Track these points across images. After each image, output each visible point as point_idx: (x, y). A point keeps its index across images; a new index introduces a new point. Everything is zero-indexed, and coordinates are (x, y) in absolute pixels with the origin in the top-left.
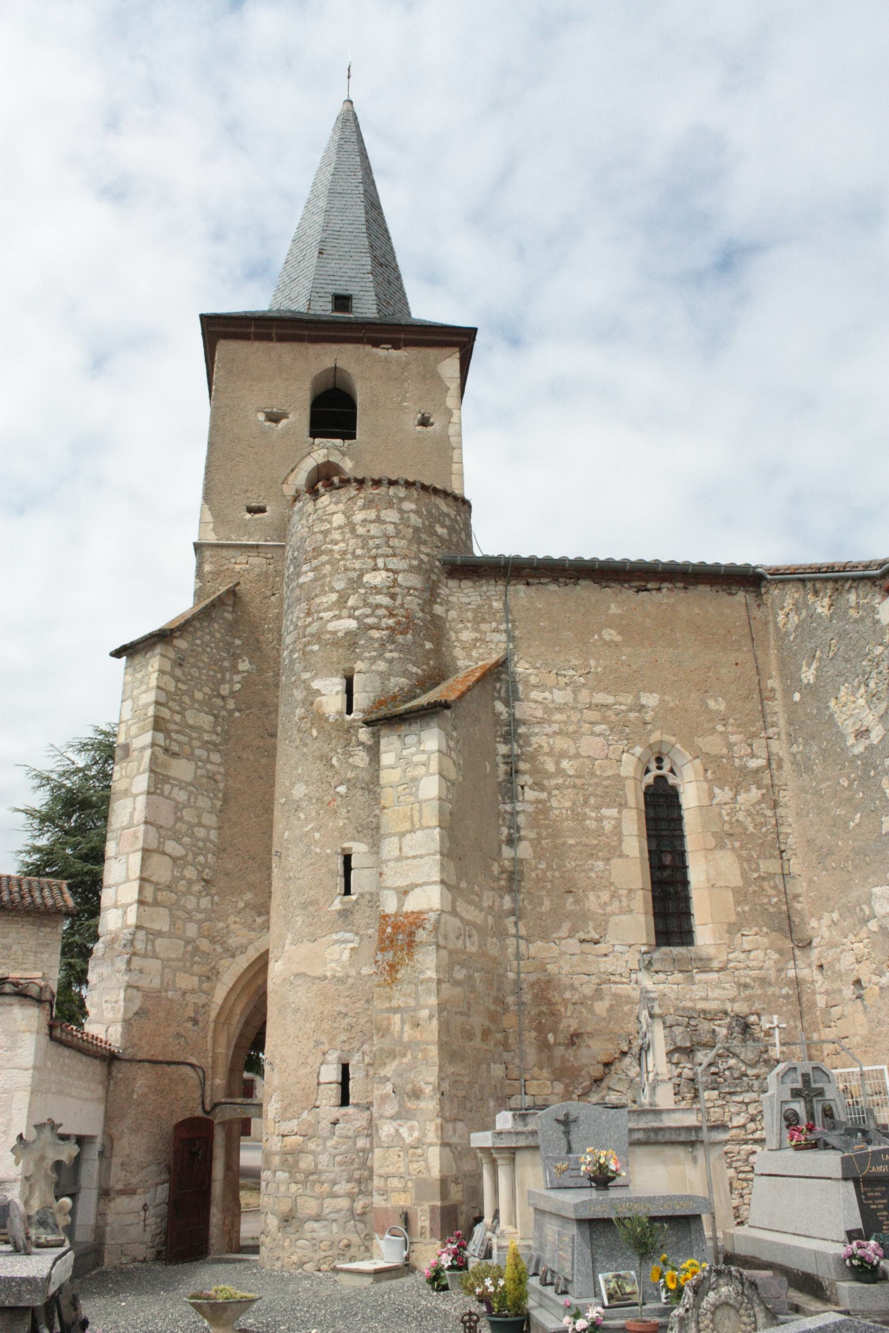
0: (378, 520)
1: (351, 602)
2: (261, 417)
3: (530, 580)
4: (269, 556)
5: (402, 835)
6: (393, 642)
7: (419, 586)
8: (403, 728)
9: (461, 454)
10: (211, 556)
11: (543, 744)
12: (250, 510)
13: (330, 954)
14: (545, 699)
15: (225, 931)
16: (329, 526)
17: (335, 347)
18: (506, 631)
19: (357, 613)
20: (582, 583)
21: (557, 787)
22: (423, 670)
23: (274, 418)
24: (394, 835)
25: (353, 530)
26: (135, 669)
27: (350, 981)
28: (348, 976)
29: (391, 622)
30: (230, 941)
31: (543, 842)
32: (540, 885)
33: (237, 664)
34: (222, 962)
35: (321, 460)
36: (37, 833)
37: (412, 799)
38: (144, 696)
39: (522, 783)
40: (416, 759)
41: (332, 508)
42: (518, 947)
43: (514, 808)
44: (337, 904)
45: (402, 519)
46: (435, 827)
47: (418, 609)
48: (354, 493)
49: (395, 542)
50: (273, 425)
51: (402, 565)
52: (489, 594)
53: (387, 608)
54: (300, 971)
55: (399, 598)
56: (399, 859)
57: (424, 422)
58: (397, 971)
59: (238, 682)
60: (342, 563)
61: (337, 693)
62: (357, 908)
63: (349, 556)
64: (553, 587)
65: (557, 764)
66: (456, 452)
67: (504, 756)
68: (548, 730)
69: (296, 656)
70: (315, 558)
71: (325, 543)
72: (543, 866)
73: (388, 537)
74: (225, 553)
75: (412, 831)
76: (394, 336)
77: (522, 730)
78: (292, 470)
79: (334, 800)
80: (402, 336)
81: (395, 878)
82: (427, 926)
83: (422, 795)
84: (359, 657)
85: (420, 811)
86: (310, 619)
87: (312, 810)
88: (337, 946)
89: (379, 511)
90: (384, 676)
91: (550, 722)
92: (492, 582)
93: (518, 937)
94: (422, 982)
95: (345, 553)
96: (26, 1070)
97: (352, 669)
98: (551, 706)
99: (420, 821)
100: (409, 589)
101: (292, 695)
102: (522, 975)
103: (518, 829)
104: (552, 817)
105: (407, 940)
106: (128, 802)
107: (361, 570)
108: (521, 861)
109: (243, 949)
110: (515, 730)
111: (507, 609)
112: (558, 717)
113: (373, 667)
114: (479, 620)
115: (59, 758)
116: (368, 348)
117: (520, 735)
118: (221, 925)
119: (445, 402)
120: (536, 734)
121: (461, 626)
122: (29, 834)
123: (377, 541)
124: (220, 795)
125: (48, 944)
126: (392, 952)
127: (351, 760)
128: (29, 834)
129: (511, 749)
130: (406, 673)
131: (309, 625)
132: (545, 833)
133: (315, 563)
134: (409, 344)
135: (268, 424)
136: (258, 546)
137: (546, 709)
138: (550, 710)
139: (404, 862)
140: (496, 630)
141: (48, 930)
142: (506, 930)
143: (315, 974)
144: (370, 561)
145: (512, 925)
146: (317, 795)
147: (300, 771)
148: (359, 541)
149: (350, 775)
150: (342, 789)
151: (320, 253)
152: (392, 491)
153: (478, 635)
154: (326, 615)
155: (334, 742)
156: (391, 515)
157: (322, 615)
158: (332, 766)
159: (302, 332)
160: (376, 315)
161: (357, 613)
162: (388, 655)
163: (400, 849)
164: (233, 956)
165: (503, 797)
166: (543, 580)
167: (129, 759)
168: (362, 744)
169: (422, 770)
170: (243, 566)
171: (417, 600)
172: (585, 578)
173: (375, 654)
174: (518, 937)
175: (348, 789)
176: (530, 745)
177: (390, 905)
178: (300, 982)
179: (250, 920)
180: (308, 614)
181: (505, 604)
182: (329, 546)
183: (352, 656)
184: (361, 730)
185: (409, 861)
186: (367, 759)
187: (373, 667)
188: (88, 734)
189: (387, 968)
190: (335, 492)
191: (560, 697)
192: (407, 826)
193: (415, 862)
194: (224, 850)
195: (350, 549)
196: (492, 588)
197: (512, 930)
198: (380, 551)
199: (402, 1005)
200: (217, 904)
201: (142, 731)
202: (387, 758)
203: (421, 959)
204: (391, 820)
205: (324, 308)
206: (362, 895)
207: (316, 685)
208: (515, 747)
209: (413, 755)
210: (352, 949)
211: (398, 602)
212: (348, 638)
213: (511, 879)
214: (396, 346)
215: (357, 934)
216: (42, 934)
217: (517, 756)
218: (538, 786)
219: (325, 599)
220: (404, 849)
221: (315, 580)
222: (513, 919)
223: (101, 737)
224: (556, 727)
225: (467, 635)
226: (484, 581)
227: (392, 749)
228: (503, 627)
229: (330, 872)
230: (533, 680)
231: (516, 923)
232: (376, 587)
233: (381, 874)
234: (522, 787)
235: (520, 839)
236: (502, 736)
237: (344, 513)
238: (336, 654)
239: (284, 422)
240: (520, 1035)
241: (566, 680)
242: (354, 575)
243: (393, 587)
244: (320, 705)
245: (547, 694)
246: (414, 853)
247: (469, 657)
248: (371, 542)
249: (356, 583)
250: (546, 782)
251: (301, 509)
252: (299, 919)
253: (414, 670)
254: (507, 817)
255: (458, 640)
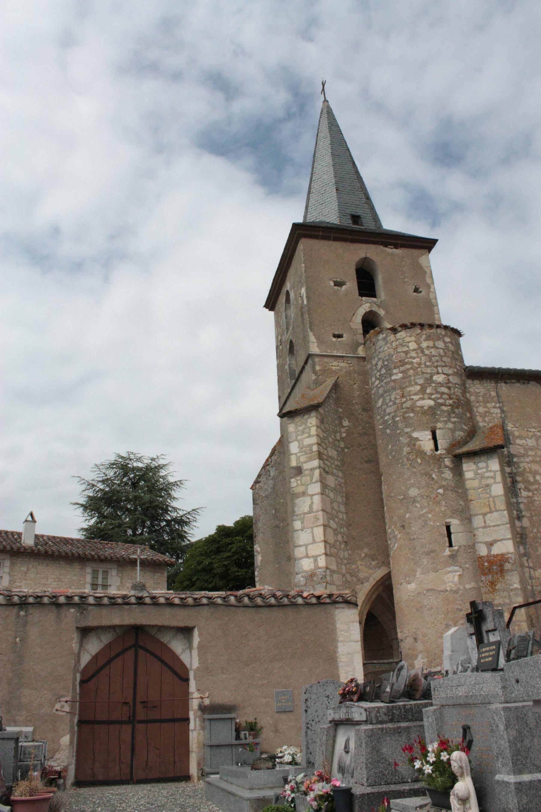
0: (435, 347)
1: (428, 391)
2: (332, 284)
3: (507, 381)
4: (349, 362)
5: (484, 515)
6: (454, 413)
7: (459, 383)
8: (476, 458)
9: (438, 309)
10: (319, 362)
11: (526, 467)
12: (335, 336)
13: (447, 578)
14: (523, 443)
15: (357, 570)
16: (407, 349)
17: (364, 246)
18: (499, 407)
19: (433, 397)
20: (532, 383)
21: (536, 490)
22: (469, 428)
23: (339, 284)
24: (480, 514)
25: (423, 352)
26: (296, 424)
27: (461, 592)
28: (459, 590)
29: (451, 402)
30: (360, 575)
31: (534, 518)
32: (536, 541)
33: (342, 422)
34: (357, 587)
35: (368, 310)
36: (89, 518)
37: (488, 496)
38: (307, 440)
39: (519, 488)
40: (486, 475)
41: (408, 339)
42: (530, 573)
43: (517, 501)
44: (447, 552)
45: (445, 346)
46: (504, 510)
47: (461, 395)
48: (420, 331)
49: (445, 359)
50: (339, 288)
51: (450, 371)
52: (488, 387)
53: (448, 394)
54: (430, 588)
55: (452, 389)
56: (485, 527)
57: (416, 290)
58: (496, 585)
59: (345, 432)
60: (419, 369)
61: (429, 440)
62: (459, 553)
63: (423, 366)
64: (518, 385)
65: (534, 477)
66: (435, 308)
67: (509, 473)
68: (528, 460)
69: (397, 419)
70: (402, 366)
71: (407, 358)
72: (535, 531)
73: (441, 357)
74: (326, 360)
75: (491, 512)
76: (394, 241)
77: (515, 460)
78: (354, 315)
79: (437, 497)
80: (400, 242)
81: (483, 536)
82: (510, 561)
83: (494, 493)
84: (438, 421)
85: (494, 502)
86: (404, 399)
87: (425, 502)
88: (450, 574)
89: (434, 341)
90: (453, 431)
91: (528, 456)
92: (489, 381)
93: (529, 567)
94: (512, 590)
95: (420, 364)
96: (357, 642)
97: (436, 427)
98: (527, 447)
99: (494, 507)
100: (456, 384)
101: (399, 440)
102: (534, 587)
103: (521, 512)
104: (536, 505)
105: (499, 568)
106: (307, 499)
107: (431, 373)
108: (525, 528)
109: (367, 579)
110: (512, 460)
111: (498, 396)
112: (530, 453)
113: (446, 426)
114: (486, 402)
115: (98, 472)
116: (382, 247)
117: (515, 462)
118: (354, 566)
119: (425, 280)
120: (522, 462)
121: (478, 404)
122: (84, 518)
123: (437, 358)
124: (344, 495)
125: (159, 583)
126: (491, 576)
127: (443, 475)
128: (84, 518)
129: (512, 470)
130: (462, 430)
131: (405, 402)
132: (534, 514)
133: (402, 369)
134: (403, 246)
135: (336, 287)
136: (343, 357)
137: (525, 449)
138: (527, 449)
139: (488, 529)
140: (494, 407)
141: (159, 574)
142: (523, 564)
143: (439, 589)
144: (435, 369)
145: (526, 561)
146: (426, 494)
147: (412, 481)
148: (427, 357)
149: (444, 483)
150: (441, 491)
151: (337, 190)
152: (439, 331)
153: (486, 409)
154: (415, 397)
155: (432, 466)
156: (440, 344)
157: (412, 397)
158: (433, 478)
159: (347, 236)
160: (374, 228)
161: (433, 397)
162: (453, 420)
163: (485, 522)
164: (362, 583)
165: (512, 495)
166: (513, 381)
167: (303, 475)
168: (447, 467)
169: (491, 481)
170: (337, 368)
171: (460, 390)
172: (532, 381)
173: (446, 419)
174: (529, 567)
175: (444, 490)
176: (520, 468)
177: (483, 551)
178: (431, 594)
179: (369, 564)
180: (403, 396)
181: (497, 393)
182: (410, 360)
183: (434, 420)
184: (446, 460)
185: (491, 528)
186: (451, 475)
187: (446, 426)
188: (112, 458)
189: (489, 584)
190: (408, 330)
191: (531, 442)
192: (487, 510)
193: (495, 528)
194: (350, 525)
195: (423, 362)
196: (489, 384)
197: (526, 564)
198: (439, 364)
199: (502, 603)
200: (351, 555)
201: (311, 459)
202: (468, 475)
203: (509, 579)
204: (476, 506)
205: (348, 223)
206: (460, 547)
207: (415, 435)
208: (514, 469)
209: (484, 473)
210: (460, 575)
211: (452, 391)
212: (430, 410)
213: (521, 538)
214: (396, 247)
215: (461, 567)
216: (155, 577)
217: (515, 473)
218: (527, 489)
219: (412, 389)
220: (487, 522)
221: (403, 378)
222: (526, 558)
223: (120, 460)
224: (530, 459)
225: (481, 410)
226: (485, 381)
227: (469, 469)
228: (498, 405)
229: (441, 534)
230: (517, 434)
231: (527, 560)
232: (440, 383)
233: (474, 535)
234: (520, 489)
235: (523, 516)
236: (506, 463)
237: (415, 342)
238: (425, 419)
239: (344, 287)
240: (538, 618)
241: (532, 434)
242: (428, 376)
243: (448, 383)
244: (420, 446)
245: (524, 441)
246: (494, 524)
247: (484, 421)
248: (433, 359)
249: (429, 380)
250: (530, 487)
251: (384, 339)
252: (424, 560)
253: (465, 428)
254: (515, 505)
255: (478, 412)
